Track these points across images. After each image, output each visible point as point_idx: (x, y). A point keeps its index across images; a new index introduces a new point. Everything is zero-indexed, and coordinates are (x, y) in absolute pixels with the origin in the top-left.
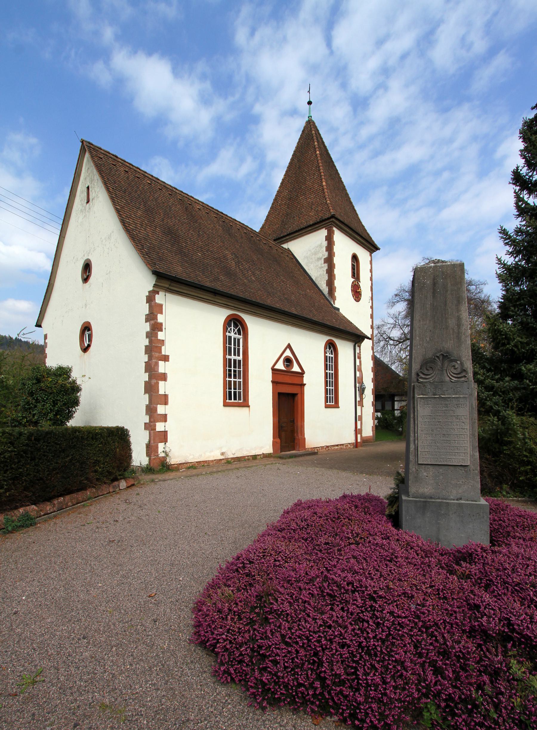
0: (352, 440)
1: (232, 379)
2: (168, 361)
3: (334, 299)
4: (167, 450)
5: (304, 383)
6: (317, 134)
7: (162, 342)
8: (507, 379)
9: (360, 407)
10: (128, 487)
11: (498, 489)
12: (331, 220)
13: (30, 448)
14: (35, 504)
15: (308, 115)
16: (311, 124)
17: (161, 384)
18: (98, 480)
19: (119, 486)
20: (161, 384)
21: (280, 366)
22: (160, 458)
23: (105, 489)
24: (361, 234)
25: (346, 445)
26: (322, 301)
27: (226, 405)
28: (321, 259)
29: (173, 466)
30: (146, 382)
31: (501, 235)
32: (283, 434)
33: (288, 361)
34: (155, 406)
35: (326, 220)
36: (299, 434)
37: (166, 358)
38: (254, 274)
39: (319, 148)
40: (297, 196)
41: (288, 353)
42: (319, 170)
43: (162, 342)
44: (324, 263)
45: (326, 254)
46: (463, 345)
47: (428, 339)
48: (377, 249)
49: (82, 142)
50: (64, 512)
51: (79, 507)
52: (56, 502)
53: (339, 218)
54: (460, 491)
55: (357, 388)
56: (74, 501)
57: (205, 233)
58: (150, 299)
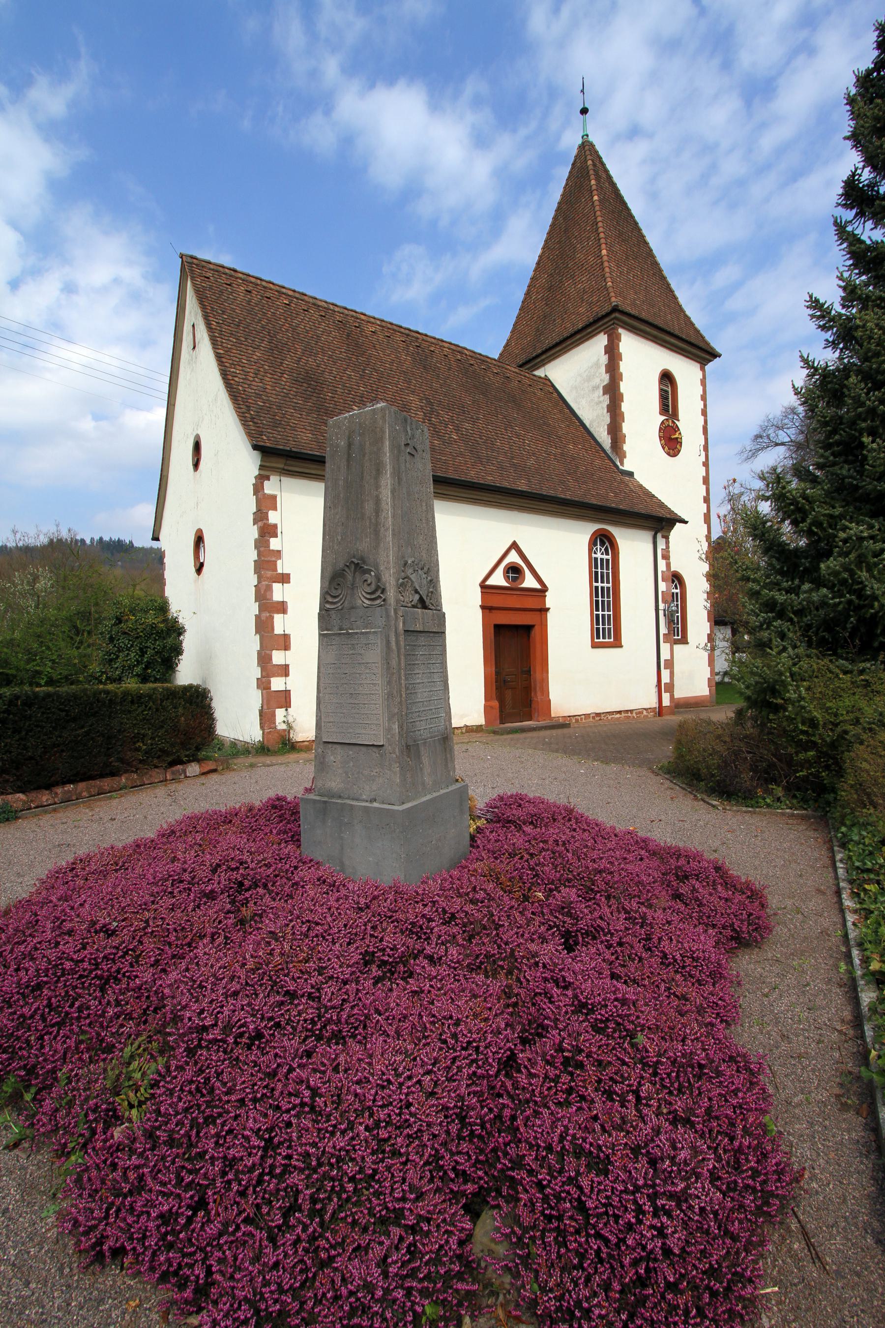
0: (653, 703)
1: (600, 613)
2: (289, 582)
3: (622, 456)
4: (291, 719)
5: (547, 606)
6: (598, 164)
7: (278, 554)
8: (806, 586)
9: (668, 645)
10: (203, 774)
11: (760, 792)
12: (613, 316)
13: (11, 716)
14: (23, 792)
15: (582, 134)
16: (587, 148)
17: (278, 618)
18: (141, 761)
19: (184, 772)
20: (278, 618)
21: (498, 579)
22: (278, 731)
23: (157, 775)
24: (677, 332)
25: (640, 712)
26: (597, 462)
27: (595, 646)
28: (598, 387)
29: (298, 744)
30: (256, 616)
31: (811, 312)
32: (509, 694)
33: (514, 571)
34: (268, 652)
35: (603, 317)
36: (539, 694)
37: (285, 579)
38: (457, 429)
39: (600, 188)
40: (561, 281)
41: (513, 557)
42: (597, 229)
43: (278, 554)
44: (604, 394)
45: (606, 379)
46: (382, 545)
47: (339, 538)
48: (714, 355)
49: (182, 256)
50: (73, 805)
51: (100, 800)
52: (59, 790)
53: (629, 309)
54: (374, 787)
55: (661, 613)
56: (94, 791)
57: (376, 371)
58: (258, 488)
